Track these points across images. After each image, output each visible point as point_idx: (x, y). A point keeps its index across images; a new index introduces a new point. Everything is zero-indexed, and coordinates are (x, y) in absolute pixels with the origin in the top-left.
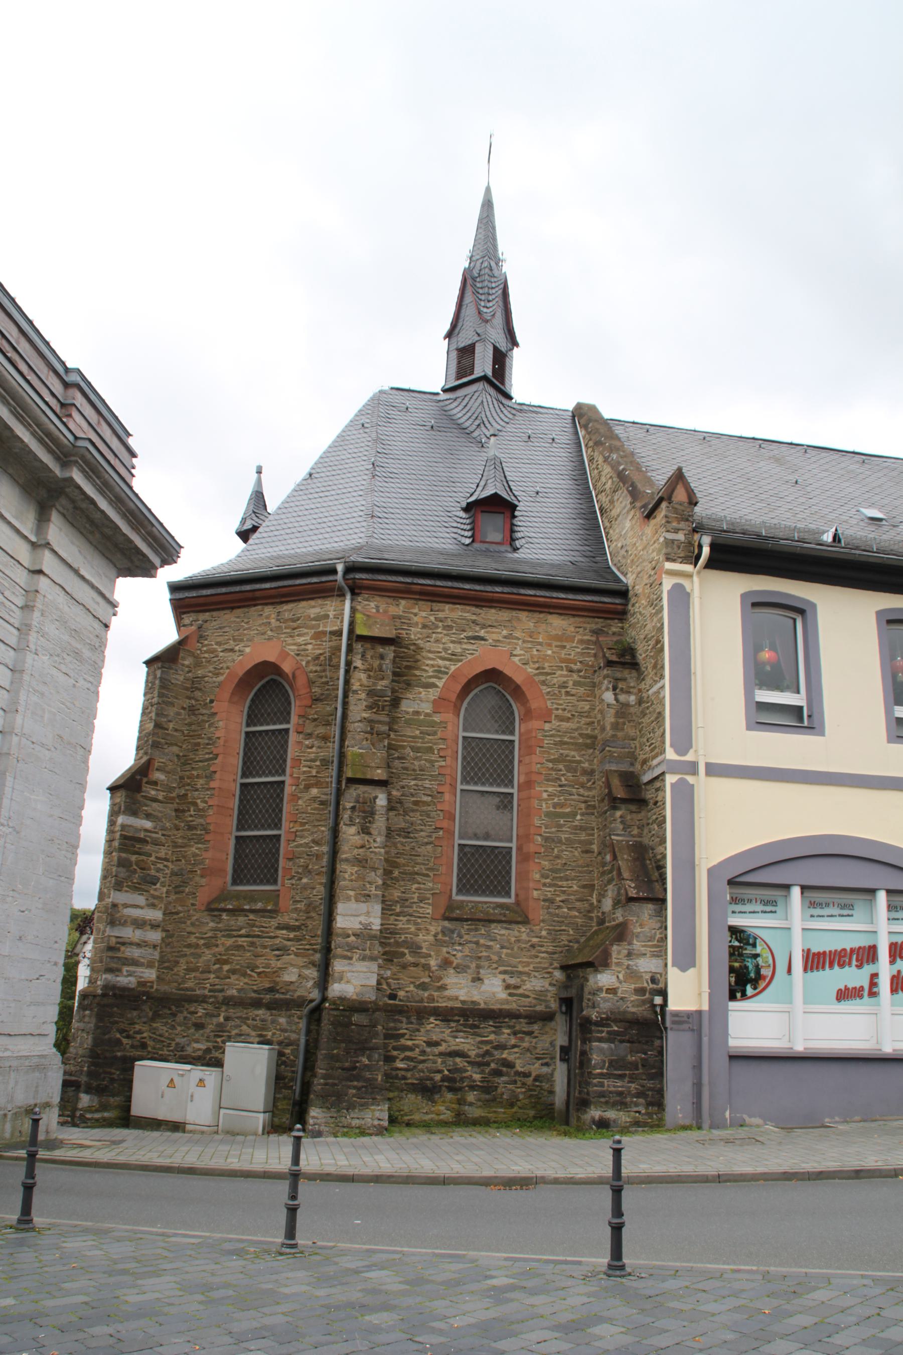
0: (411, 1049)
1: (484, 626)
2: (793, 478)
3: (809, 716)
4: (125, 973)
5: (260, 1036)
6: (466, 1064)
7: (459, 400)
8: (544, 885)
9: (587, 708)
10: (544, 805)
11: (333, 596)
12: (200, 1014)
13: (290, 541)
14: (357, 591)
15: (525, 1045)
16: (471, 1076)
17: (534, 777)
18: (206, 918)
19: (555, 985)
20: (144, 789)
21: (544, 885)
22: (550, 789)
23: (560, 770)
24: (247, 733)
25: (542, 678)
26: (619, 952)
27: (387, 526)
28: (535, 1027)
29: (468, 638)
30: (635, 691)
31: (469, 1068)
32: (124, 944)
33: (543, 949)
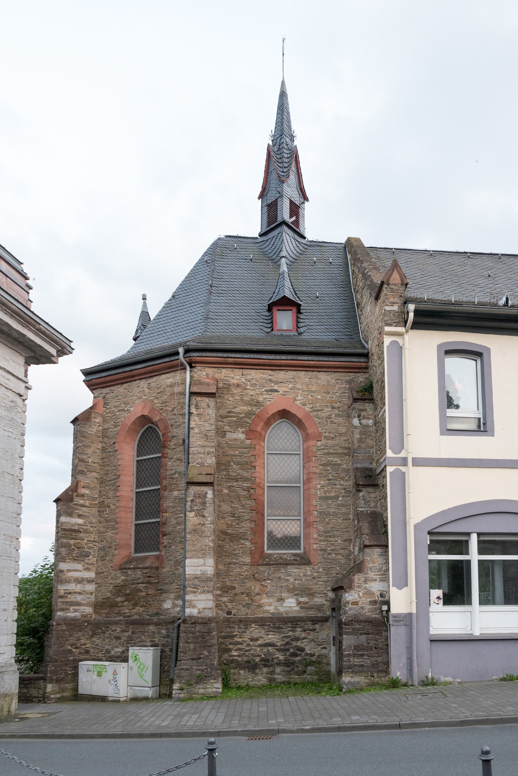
0: (241, 644)
1: (277, 383)
2: (486, 274)
3: (484, 424)
4: (72, 611)
5: (152, 641)
6: (275, 651)
7: (269, 241)
8: (320, 541)
9: (344, 430)
10: (318, 492)
11: (178, 370)
12: (118, 631)
13: (159, 340)
14: (193, 365)
15: (311, 637)
16: (279, 657)
17: (312, 475)
18: (118, 573)
19: (328, 601)
20: (75, 500)
21: (320, 541)
22: (322, 483)
23: (328, 470)
24: (138, 461)
25: (315, 413)
26: (359, 579)
27: (217, 324)
28: (317, 626)
29: (267, 391)
30: (373, 417)
31: (277, 653)
32: (70, 593)
33: (321, 579)
